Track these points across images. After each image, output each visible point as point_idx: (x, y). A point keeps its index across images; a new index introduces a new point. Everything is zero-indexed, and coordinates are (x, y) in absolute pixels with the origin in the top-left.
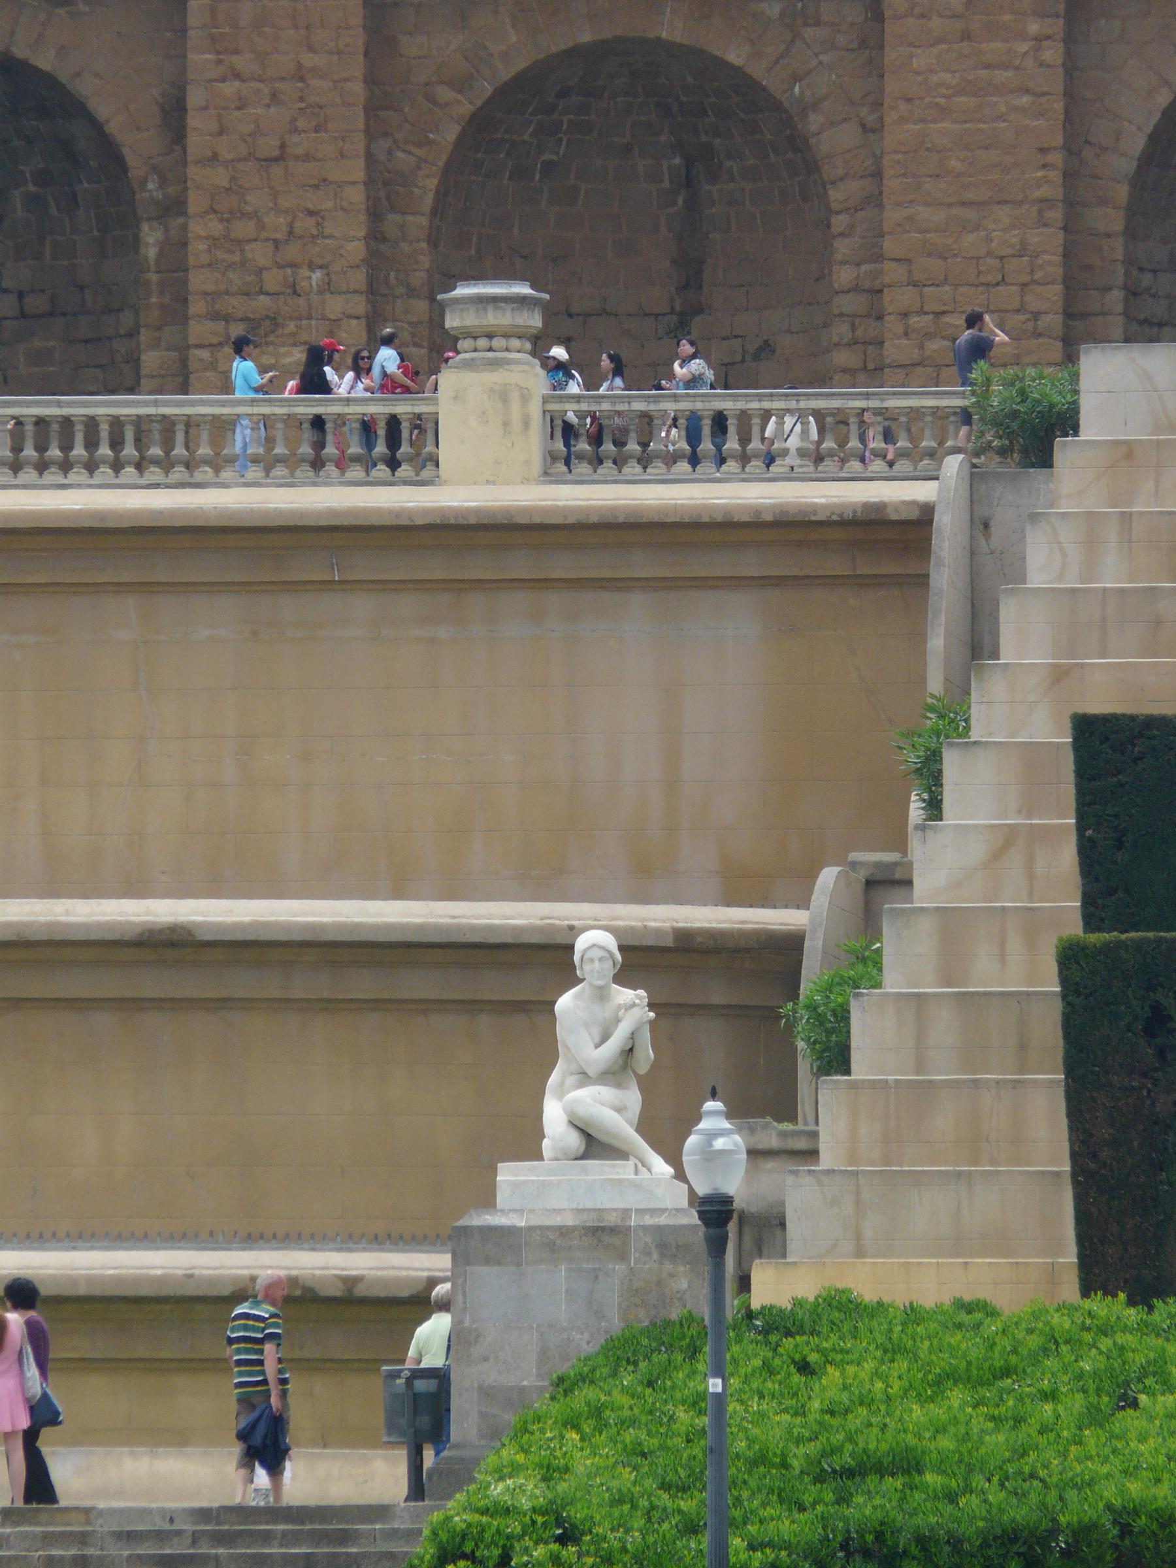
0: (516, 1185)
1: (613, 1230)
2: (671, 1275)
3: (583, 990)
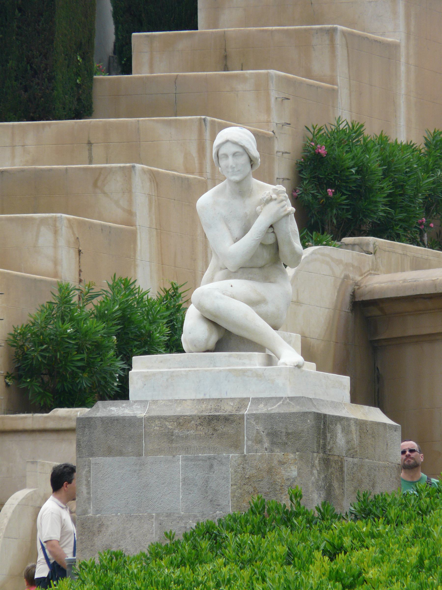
0: (146, 377)
1: (227, 419)
2: (281, 463)
3: (225, 186)
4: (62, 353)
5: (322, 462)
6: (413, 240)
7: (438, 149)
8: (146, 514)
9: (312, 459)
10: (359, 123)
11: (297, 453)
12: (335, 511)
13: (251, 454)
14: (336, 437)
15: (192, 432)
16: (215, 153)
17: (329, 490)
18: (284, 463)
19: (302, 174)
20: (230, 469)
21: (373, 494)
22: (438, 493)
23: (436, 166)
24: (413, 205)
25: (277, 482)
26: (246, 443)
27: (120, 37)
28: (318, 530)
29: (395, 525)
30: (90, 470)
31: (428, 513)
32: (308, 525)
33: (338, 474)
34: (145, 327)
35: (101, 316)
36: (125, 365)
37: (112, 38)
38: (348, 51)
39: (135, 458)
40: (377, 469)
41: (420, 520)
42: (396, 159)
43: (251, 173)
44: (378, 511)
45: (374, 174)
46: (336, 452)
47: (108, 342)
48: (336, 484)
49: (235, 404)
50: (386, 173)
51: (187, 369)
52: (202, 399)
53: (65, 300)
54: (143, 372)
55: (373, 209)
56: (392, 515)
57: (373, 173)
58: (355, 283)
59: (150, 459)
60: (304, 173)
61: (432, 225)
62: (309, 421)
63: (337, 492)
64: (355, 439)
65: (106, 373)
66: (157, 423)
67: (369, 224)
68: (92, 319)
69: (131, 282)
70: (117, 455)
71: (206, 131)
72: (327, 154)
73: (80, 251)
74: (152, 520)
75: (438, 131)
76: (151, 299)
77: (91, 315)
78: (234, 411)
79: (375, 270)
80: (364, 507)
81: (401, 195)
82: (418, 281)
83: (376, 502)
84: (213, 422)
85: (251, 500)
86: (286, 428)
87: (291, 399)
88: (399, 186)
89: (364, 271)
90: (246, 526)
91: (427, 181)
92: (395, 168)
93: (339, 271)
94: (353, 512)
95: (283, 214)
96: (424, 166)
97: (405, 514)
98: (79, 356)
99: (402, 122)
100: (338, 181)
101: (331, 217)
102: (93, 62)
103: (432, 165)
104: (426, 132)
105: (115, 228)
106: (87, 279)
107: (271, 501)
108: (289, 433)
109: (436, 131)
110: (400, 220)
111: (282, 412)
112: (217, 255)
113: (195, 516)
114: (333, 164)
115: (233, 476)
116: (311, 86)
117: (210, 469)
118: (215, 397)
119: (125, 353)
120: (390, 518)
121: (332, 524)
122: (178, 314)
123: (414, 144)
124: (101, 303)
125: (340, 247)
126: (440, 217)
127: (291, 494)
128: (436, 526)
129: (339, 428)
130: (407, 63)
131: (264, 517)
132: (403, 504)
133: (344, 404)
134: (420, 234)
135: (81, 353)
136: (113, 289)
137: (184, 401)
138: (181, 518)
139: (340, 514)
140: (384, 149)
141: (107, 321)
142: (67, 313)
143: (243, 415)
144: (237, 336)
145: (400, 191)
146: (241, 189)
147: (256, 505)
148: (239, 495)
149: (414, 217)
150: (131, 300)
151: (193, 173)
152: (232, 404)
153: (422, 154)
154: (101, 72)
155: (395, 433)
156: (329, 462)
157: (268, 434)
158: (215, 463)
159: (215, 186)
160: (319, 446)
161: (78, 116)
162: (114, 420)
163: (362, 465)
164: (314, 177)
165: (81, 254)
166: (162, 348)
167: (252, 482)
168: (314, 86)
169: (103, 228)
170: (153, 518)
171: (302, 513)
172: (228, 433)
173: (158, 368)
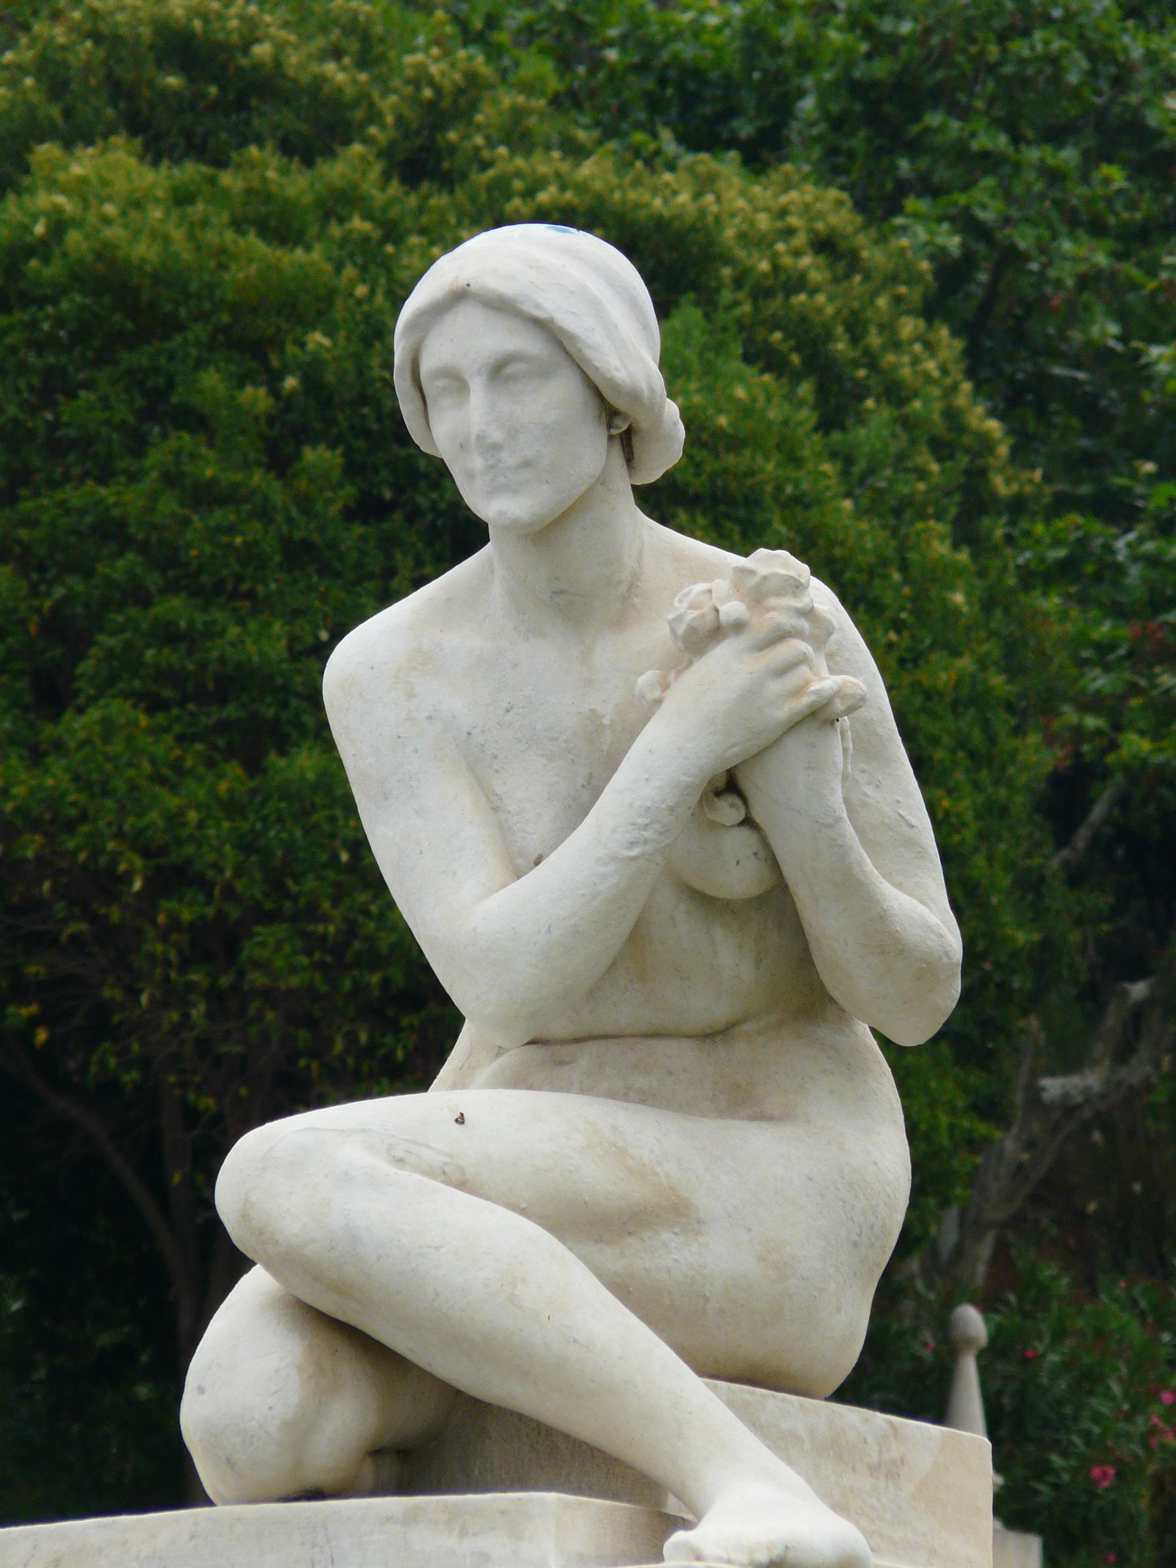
95: (784, 712)
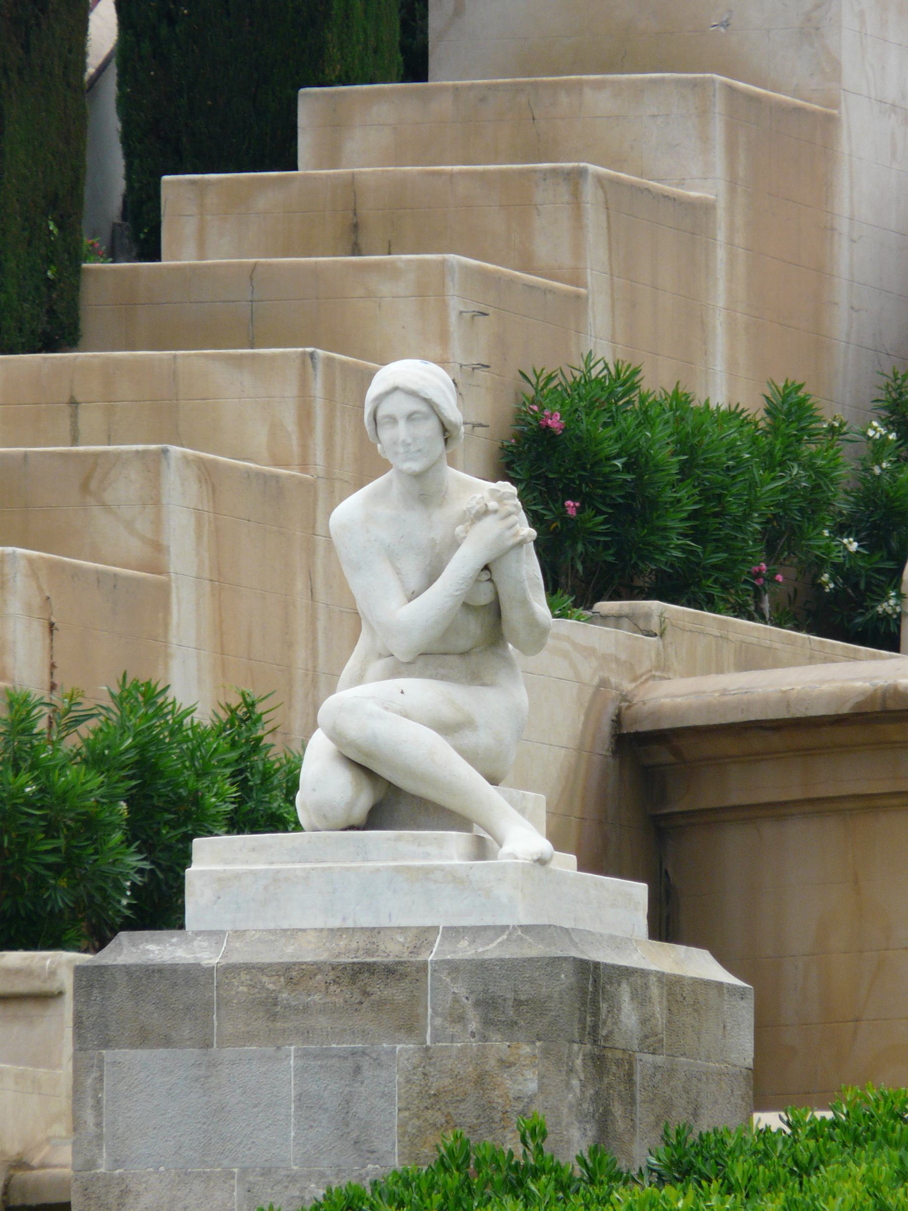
0: (222, 881)
1: (391, 972)
2: (505, 1064)
3: (390, 482)
4: (14, 835)
5: (590, 1063)
6: (740, 609)
7: (792, 422)
8: (219, 1169)
9: (569, 1056)
10: (629, 366)
11: (538, 1044)
12: (617, 1166)
13: (440, 1044)
14: (619, 1010)
15: (317, 997)
16: (369, 414)
17: (604, 1122)
18: (511, 1065)
19: (512, 469)
20: (397, 1076)
21: (696, 1132)
22: (834, 1129)
23: (788, 456)
24: (740, 536)
25: (494, 1105)
26: (431, 1022)
27: (136, 185)
28: (581, 1205)
29: (744, 1194)
30: (102, 1075)
31: (812, 1172)
32: (561, 1195)
33: (622, 1088)
34: (186, 783)
35: (95, 760)
36: (145, 863)
37: (119, 185)
38: (608, 217)
39: (196, 1051)
40: (704, 1078)
41: (797, 1186)
42: (706, 440)
43: (445, 456)
44: (707, 1167)
45: (663, 470)
46: (619, 1041)
47: (111, 815)
48: (618, 1110)
49: (409, 940)
50: (685, 470)
51: (308, 866)
52: (339, 929)
53: (21, 726)
54: (216, 871)
55: (660, 542)
56: (739, 1175)
57: (658, 468)
58: (621, 694)
59: (229, 1053)
60: (517, 469)
61: (780, 578)
62: (563, 976)
63: (621, 1125)
64: (658, 1016)
65: (105, 878)
66: (243, 979)
67: (650, 573)
68: (75, 767)
69: (159, 689)
70: (158, 1046)
71: (315, 379)
72: (565, 430)
73: (52, 625)
74: (232, 1182)
75: (793, 384)
76: (198, 726)
77: (75, 757)
78: (407, 954)
79: (662, 669)
80: (677, 1157)
81: (716, 515)
82: (752, 693)
83: (702, 1147)
84: (361, 977)
85: (439, 1142)
86: (515, 991)
87: (526, 929)
88: (712, 495)
89: (639, 672)
90: (430, 1196)
91: (771, 487)
92: (705, 459)
93: (589, 672)
94: (655, 1167)
95: (511, 542)
96: (764, 455)
97: (764, 1173)
98: (47, 844)
99: (719, 365)
100: (587, 486)
101: (573, 559)
102: (81, 235)
103: (780, 454)
104: (770, 385)
105: (127, 579)
106: (67, 684)
107: (482, 1144)
108: (520, 1001)
109: (789, 384)
110: (714, 567)
111: (507, 957)
112: (370, 627)
113: (322, 1175)
114: (575, 450)
115: (403, 1091)
116: (531, 287)
117: (355, 1076)
118: (365, 925)
119: (144, 837)
120: (733, 1180)
121: (610, 1193)
122: (256, 758)
123: (743, 411)
124: (95, 733)
125: (589, 620)
126: (796, 560)
127: (522, 1130)
128: (830, 1197)
129: (625, 993)
130: (730, 243)
131: (467, 1177)
132: (759, 1152)
133: (637, 941)
134: (755, 597)
135: (53, 837)
136: (121, 703)
137: (300, 933)
138: (293, 1179)
139: (628, 1173)
140: (683, 419)
141: (108, 770)
142: (24, 754)
143: (426, 962)
144: (413, 796)
145: (714, 507)
146: (424, 490)
147: (451, 1153)
148: (414, 1131)
149: (744, 561)
150: (158, 727)
151: (286, 465)
152: (401, 940)
153: (760, 432)
154: (96, 255)
155: (742, 1003)
156: (604, 1062)
157: (477, 1004)
158: (365, 1063)
159: (361, 486)
160: (584, 1028)
161: (49, 345)
162: (153, 972)
163: (673, 1069)
164: (537, 477)
165: (55, 632)
166: (222, 827)
167: (442, 1104)
168: (539, 288)
169: (100, 576)
170: (234, 1178)
171: (547, 1169)
172: (393, 1000)
173: (247, 862)
